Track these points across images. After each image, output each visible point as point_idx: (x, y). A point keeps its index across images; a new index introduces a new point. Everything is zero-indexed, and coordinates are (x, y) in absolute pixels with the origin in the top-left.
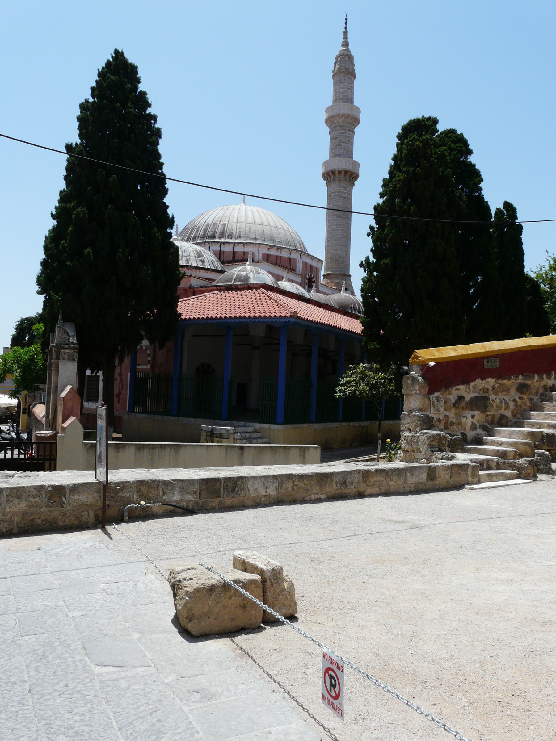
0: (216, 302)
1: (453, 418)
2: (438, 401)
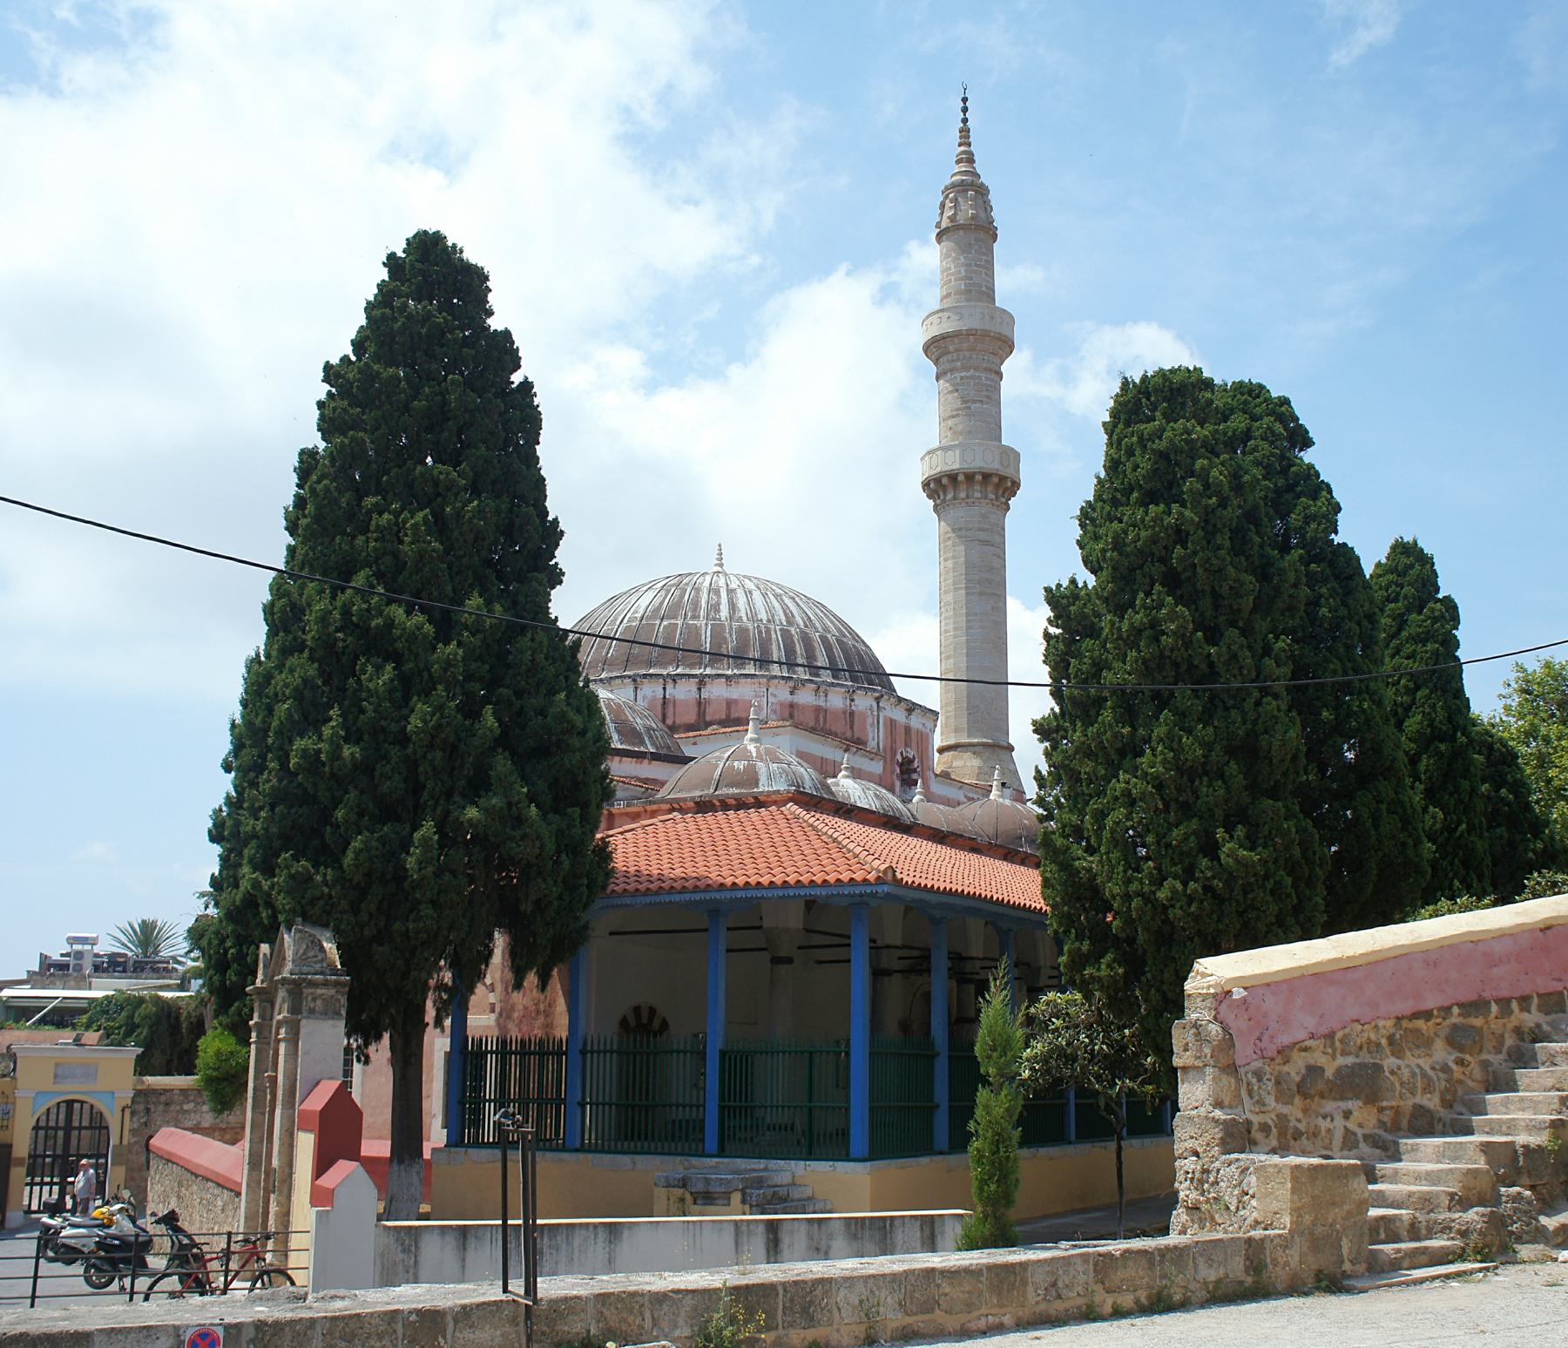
0: (674, 844)
1: (1299, 1121)
2: (1260, 1080)
